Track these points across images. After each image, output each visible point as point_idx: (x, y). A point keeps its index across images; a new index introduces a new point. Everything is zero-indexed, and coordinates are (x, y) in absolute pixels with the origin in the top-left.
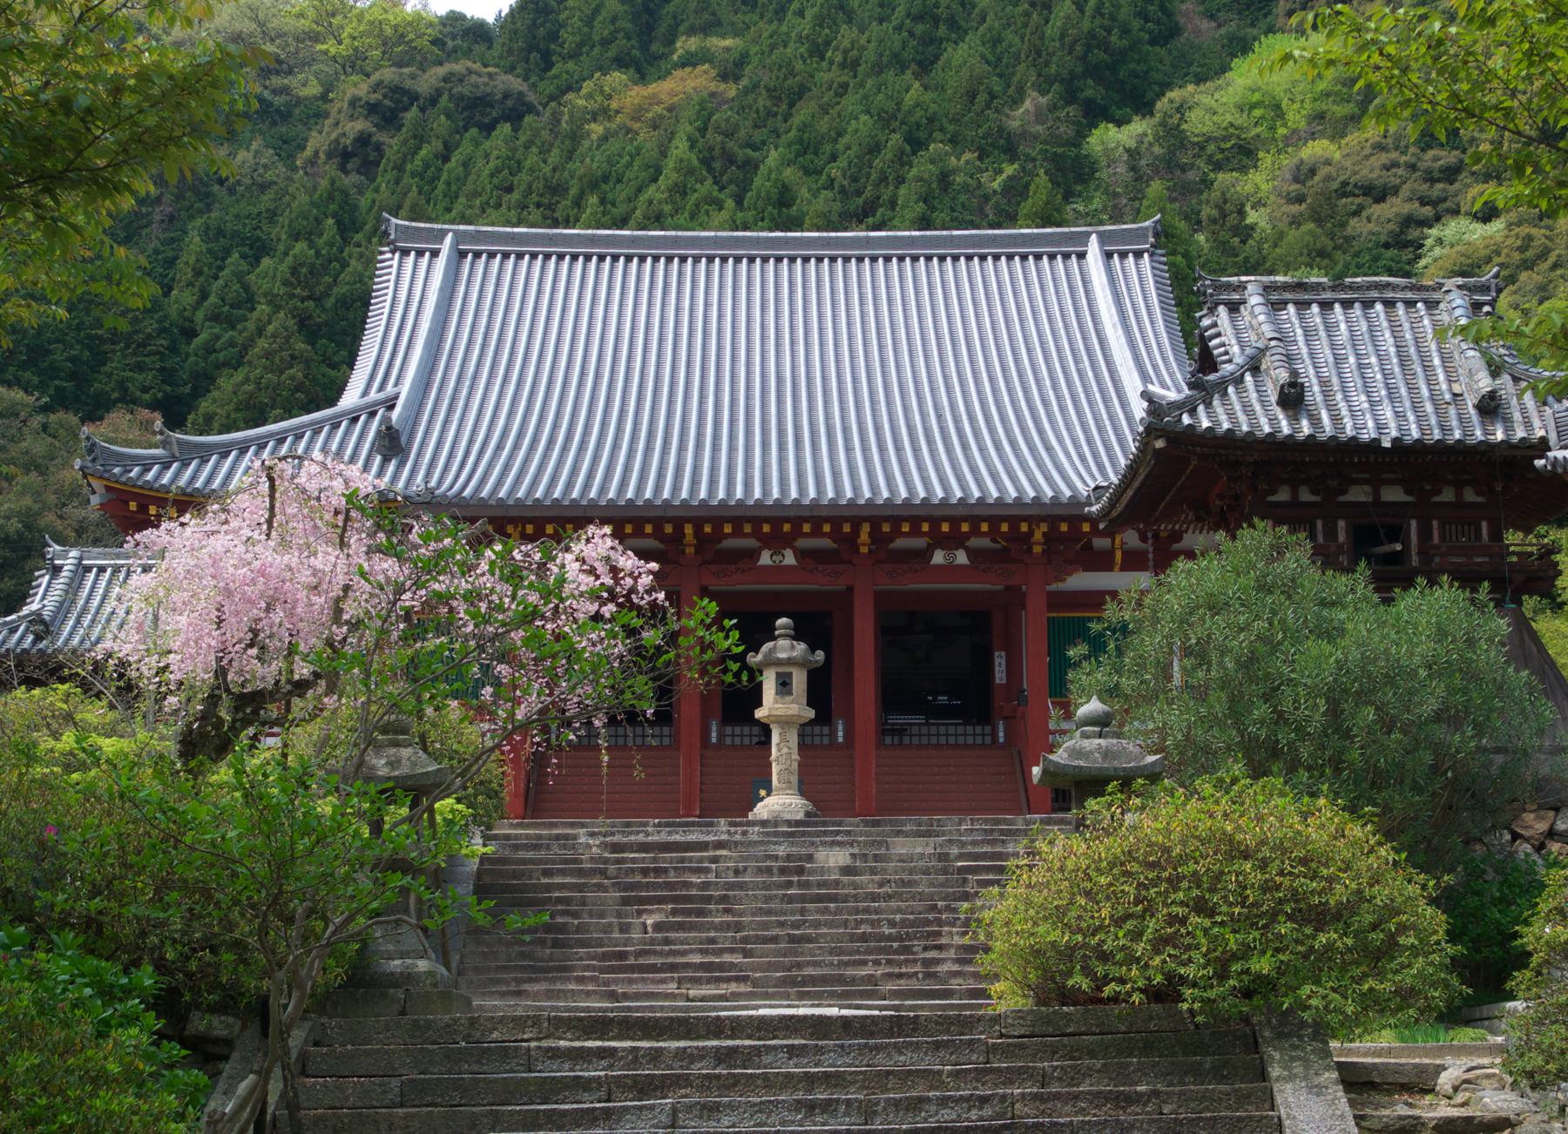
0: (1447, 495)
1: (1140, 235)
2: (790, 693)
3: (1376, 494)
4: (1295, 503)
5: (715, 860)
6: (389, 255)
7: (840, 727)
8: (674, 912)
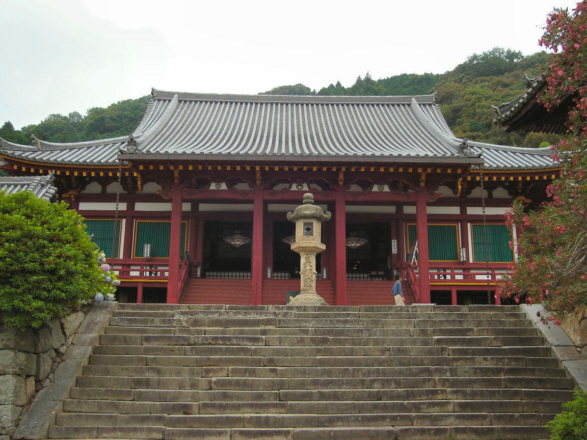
2: (312, 234)
5: (264, 332)
6: (153, 102)
7: (325, 272)
8: (235, 372)
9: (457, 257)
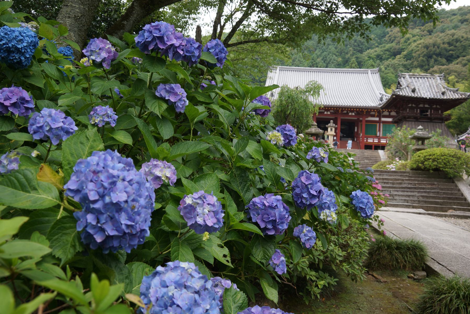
0: (435, 106)
1: (376, 70)
3: (424, 106)
4: (412, 106)
9: (376, 134)
